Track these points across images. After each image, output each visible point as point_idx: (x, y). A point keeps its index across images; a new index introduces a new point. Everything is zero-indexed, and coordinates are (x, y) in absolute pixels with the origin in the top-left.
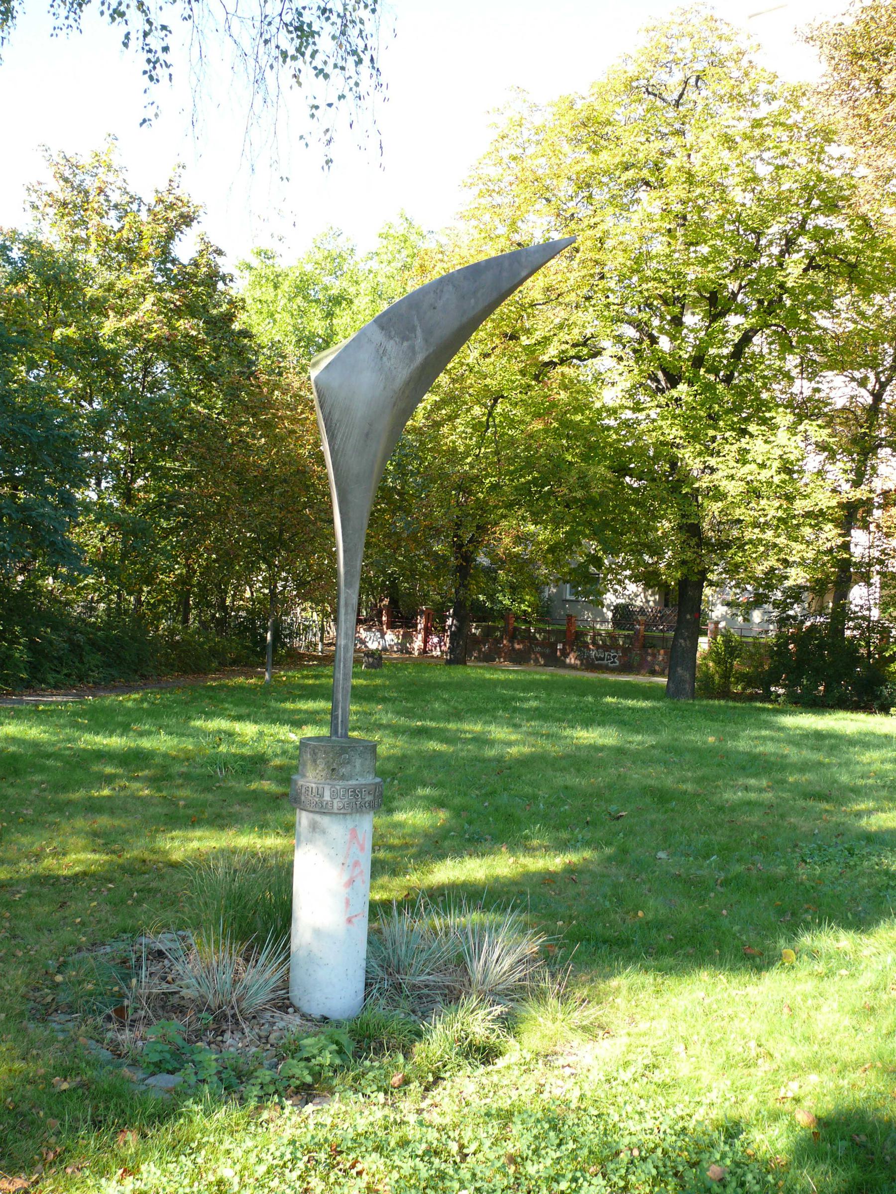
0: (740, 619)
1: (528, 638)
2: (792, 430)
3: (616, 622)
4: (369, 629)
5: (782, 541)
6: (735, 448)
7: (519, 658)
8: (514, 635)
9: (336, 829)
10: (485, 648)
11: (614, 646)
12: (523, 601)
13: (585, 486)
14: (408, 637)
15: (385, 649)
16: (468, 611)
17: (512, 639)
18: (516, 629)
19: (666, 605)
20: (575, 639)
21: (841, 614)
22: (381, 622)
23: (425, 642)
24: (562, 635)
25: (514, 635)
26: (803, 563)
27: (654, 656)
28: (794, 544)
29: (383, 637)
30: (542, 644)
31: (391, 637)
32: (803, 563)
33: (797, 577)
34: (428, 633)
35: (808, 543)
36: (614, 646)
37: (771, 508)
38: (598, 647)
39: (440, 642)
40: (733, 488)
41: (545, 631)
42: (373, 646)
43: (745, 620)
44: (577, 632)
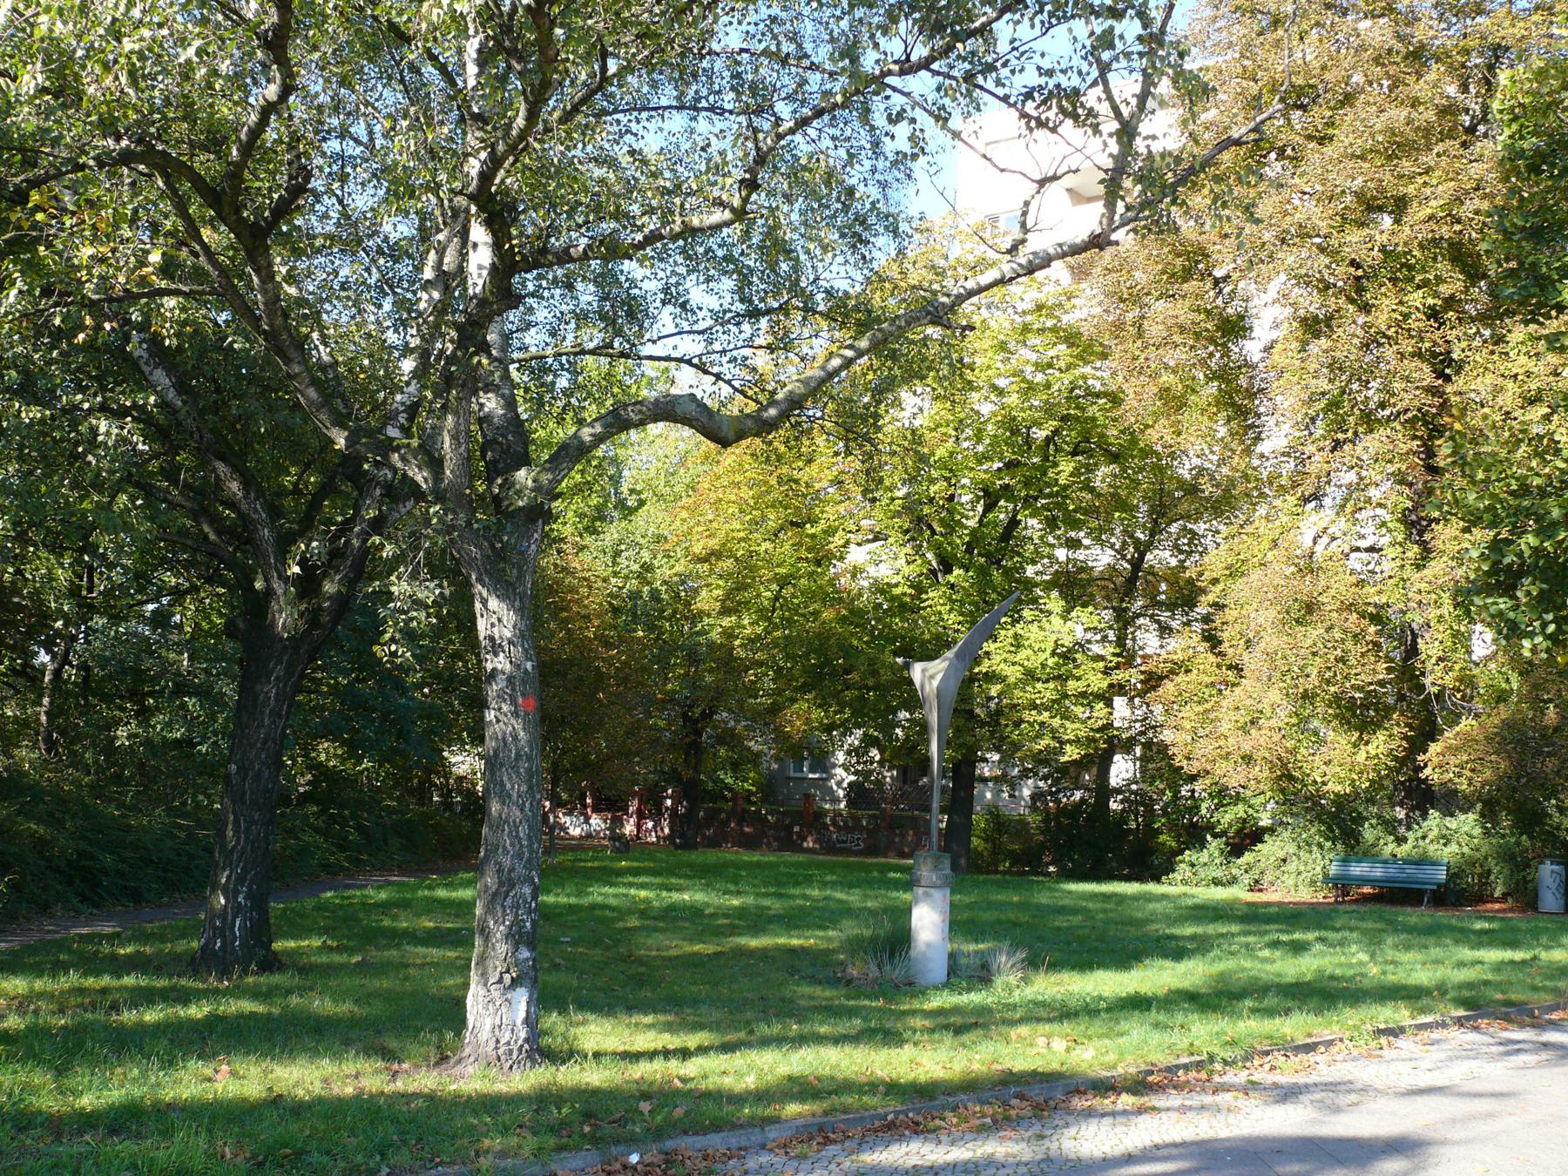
0: (1006, 795)
1: (757, 819)
2: (1065, 616)
3: (851, 803)
4: (570, 814)
5: (1056, 722)
6: (1011, 633)
7: (750, 843)
8: (743, 818)
9: (937, 894)
10: (709, 832)
11: (857, 827)
12: (745, 780)
13: (875, 673)
14: (617, 822)
15: (589, 836)
16: (690, 791)
17: (740, 822)
18: (745, 811)
19: (905, 782)
20: (813, 819)
21: (1103, 790)
22: (585, 806)
23: (639, 827)
24: (798, 816)
25: (743, 818)
26: (1077, 741)
27: (903, 836)
28: (1068, 724)
29: (587, 821)
30: (775, 827)
31: (596, 822)
32: (1077, 741)
33: (1071, 753)
34: (641, 816)
35: (1084, 722)
36: (857, 827)
37: (1047, 691)
38: (839, 829)
39: (655, 827)
40: (1013, 673)
41: (779, 812)
42: (575, 832)
43: (1011, 796)
44: (815, 813)
